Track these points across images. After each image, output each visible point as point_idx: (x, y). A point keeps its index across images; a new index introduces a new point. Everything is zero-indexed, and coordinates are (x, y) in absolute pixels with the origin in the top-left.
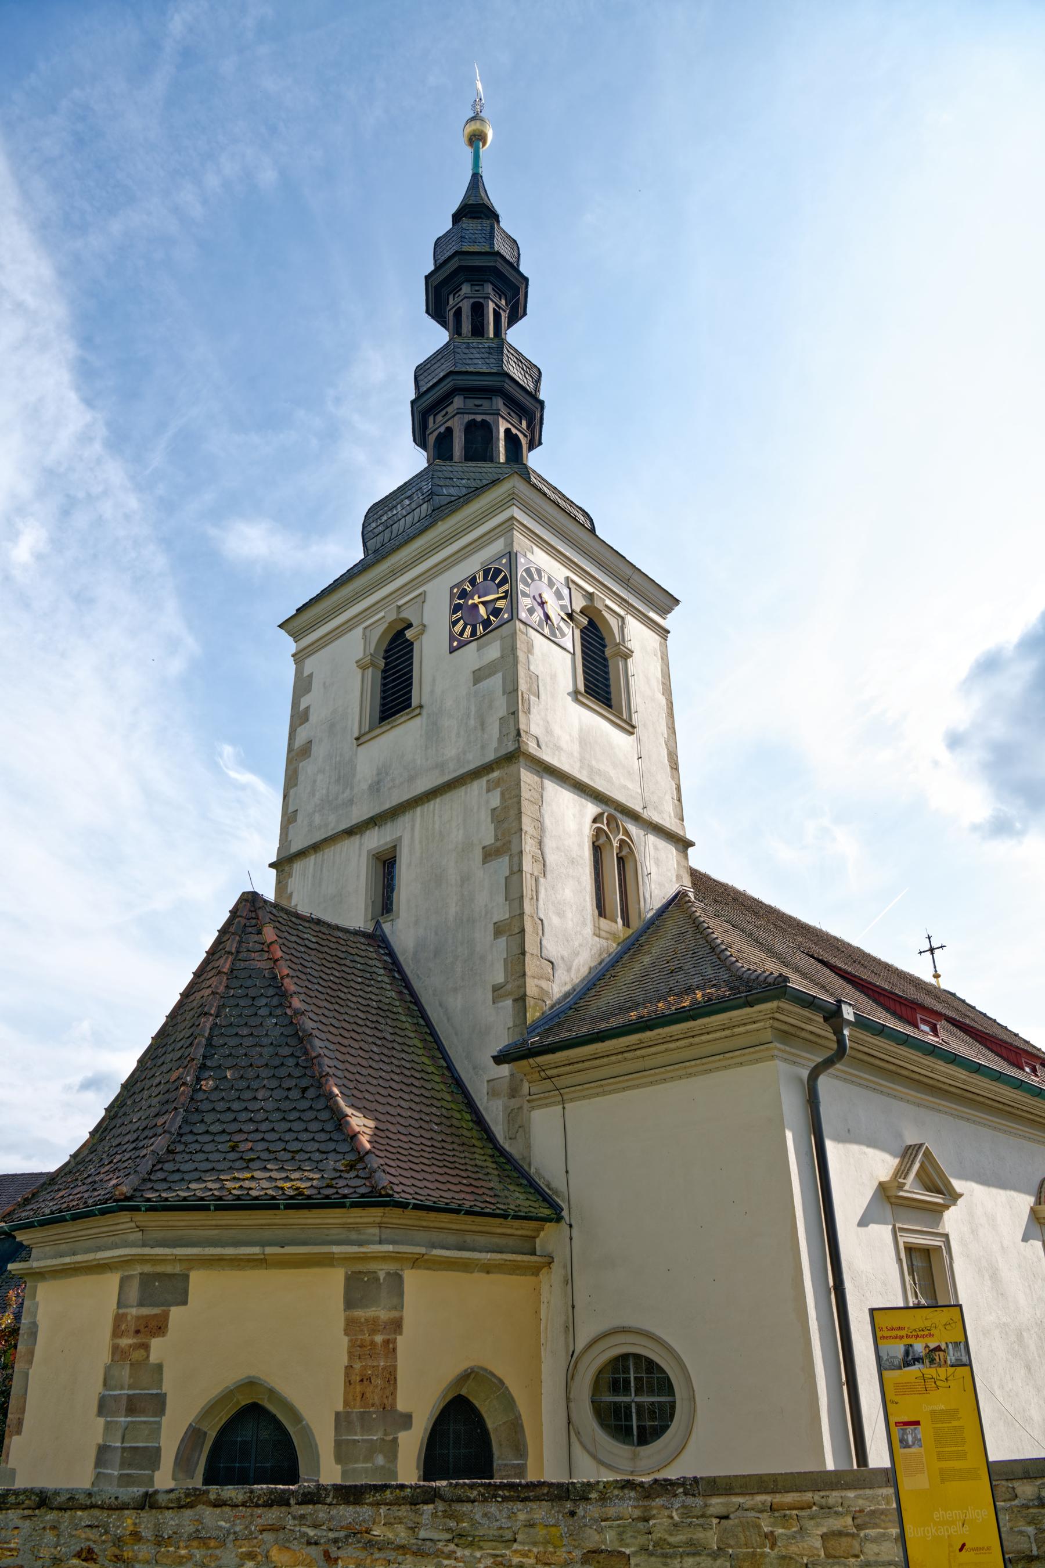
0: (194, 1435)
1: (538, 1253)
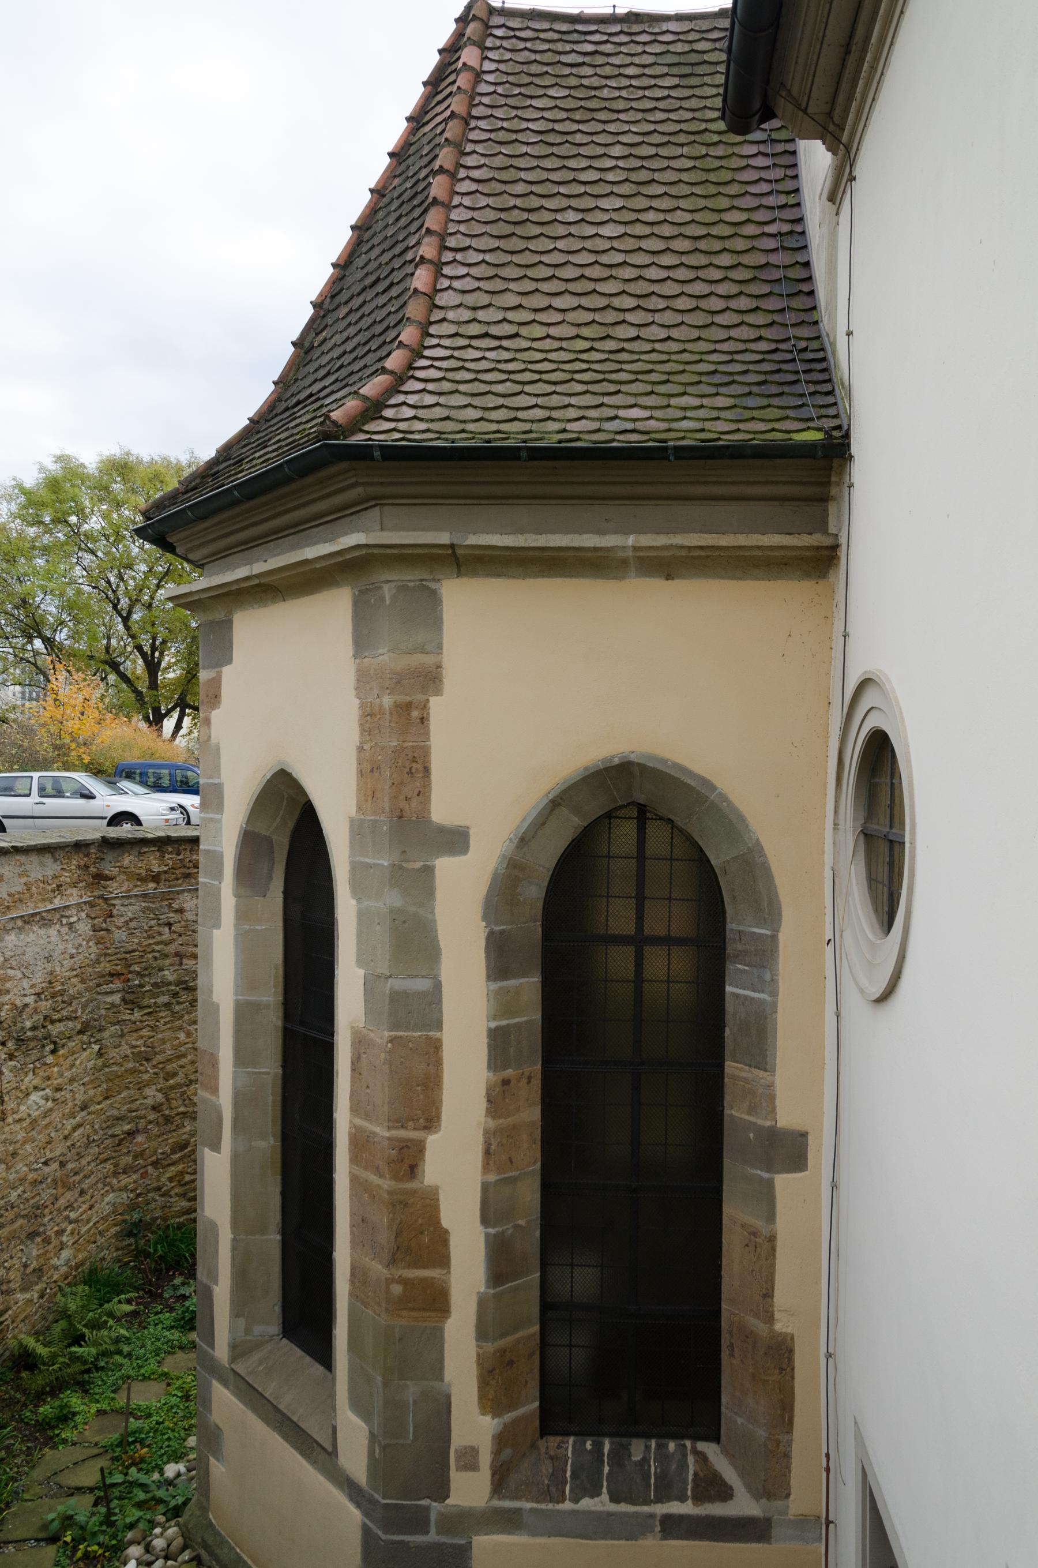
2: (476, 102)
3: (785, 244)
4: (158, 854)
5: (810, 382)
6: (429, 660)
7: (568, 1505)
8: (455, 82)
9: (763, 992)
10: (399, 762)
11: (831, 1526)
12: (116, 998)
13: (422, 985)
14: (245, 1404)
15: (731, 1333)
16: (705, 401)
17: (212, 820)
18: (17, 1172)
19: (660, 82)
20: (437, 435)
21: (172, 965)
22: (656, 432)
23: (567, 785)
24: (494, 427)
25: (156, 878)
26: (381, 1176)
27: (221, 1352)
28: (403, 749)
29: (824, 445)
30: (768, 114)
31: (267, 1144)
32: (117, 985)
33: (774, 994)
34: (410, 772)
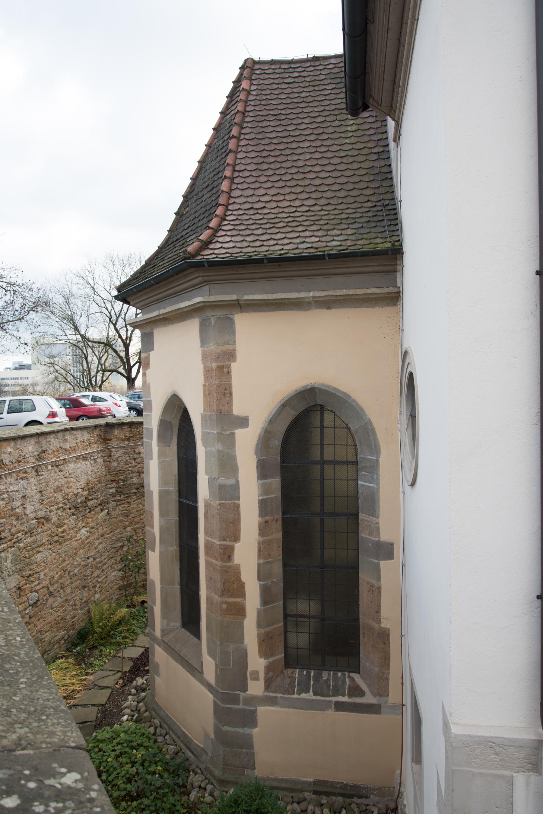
0: (163, 424)
2: (248, 104)
3: (381, 157)
4: (129, 429)
5: (389, 220)
6: (230, 347)
7: (296, 696)
8: (239, 96)
9: (373, 483)
10: (220, 389)
11: (404, 707)
12: (113, 490)
13: (231, 482)
14: (168, 654)
15: (363, 628)
16: (343, 232)
17: (148, 415)
18: (77, 561)
19: (327, 87)
20: (230, 255)
22: (320, 248)
23: (289, 397)
24: (253, 249)
25: (128, 439)
26: (217, 560)
27: (158, 633)
28: (221, 385)
29: (391, 250)
30: (365, 107)
31: (174, 549)
32: (114, 485)
33: (378, 484)
34: (224, 394)
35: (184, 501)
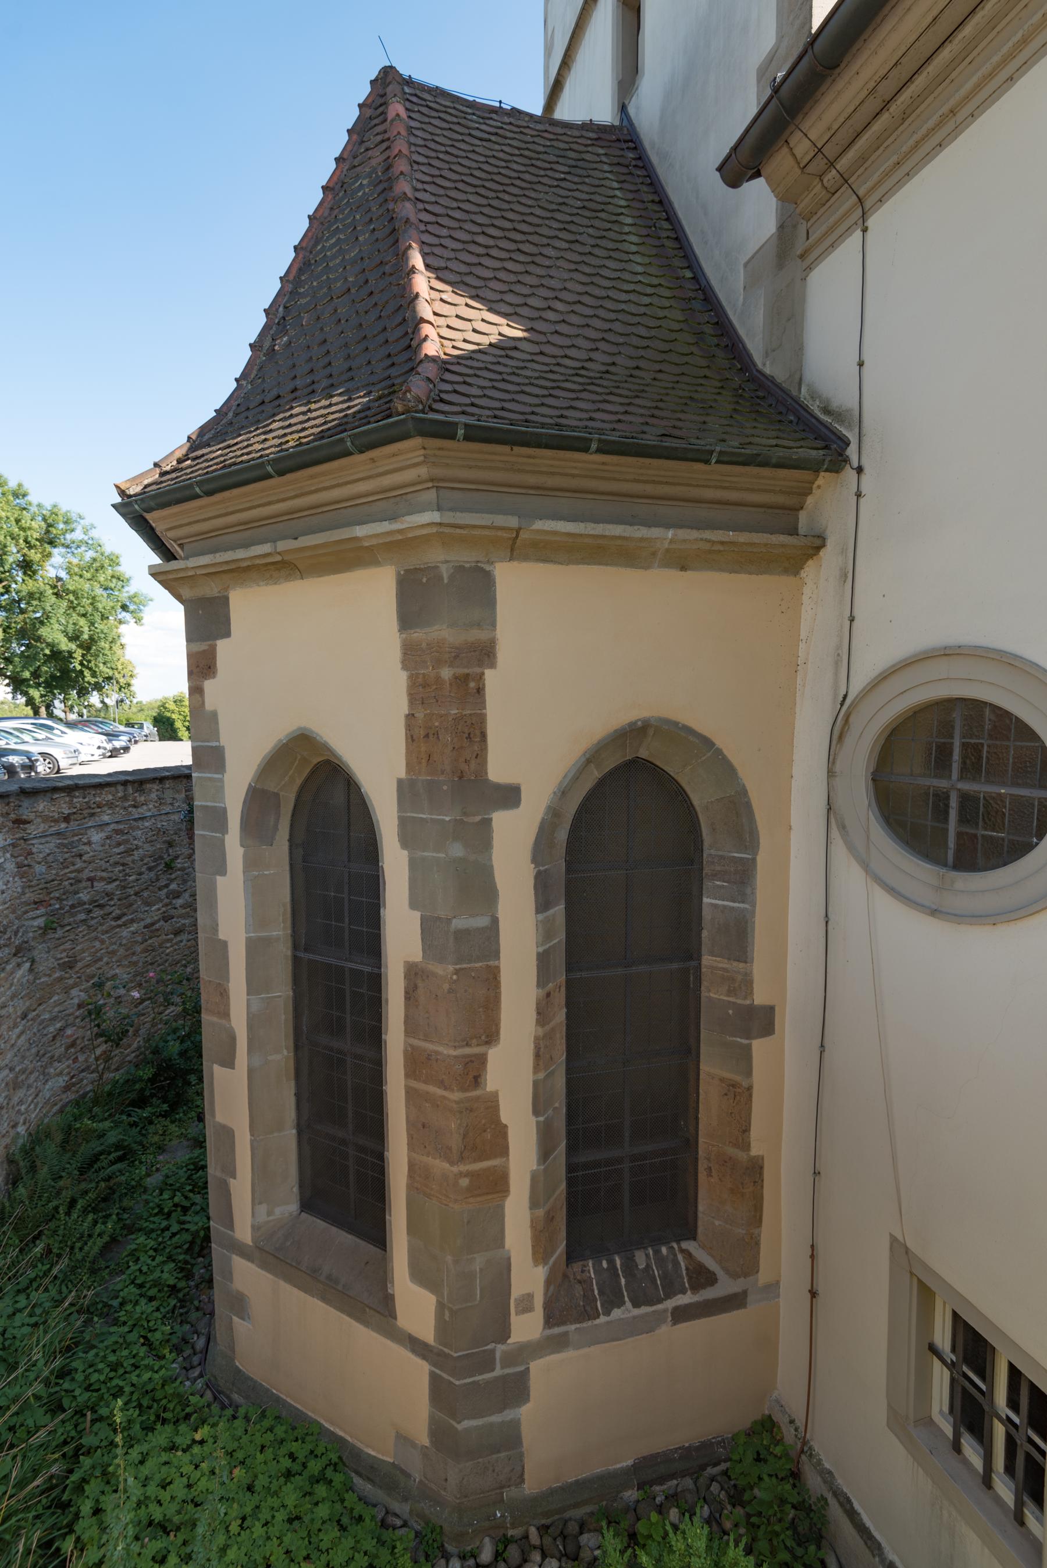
0: (259, 799)
1: (802, 530)
4: (67, 799)
7: (603, 1319)
13: (482, 922)
21: (85, 888)
25: (67, 819)
33: (754, 905)
35: (301, 955)
